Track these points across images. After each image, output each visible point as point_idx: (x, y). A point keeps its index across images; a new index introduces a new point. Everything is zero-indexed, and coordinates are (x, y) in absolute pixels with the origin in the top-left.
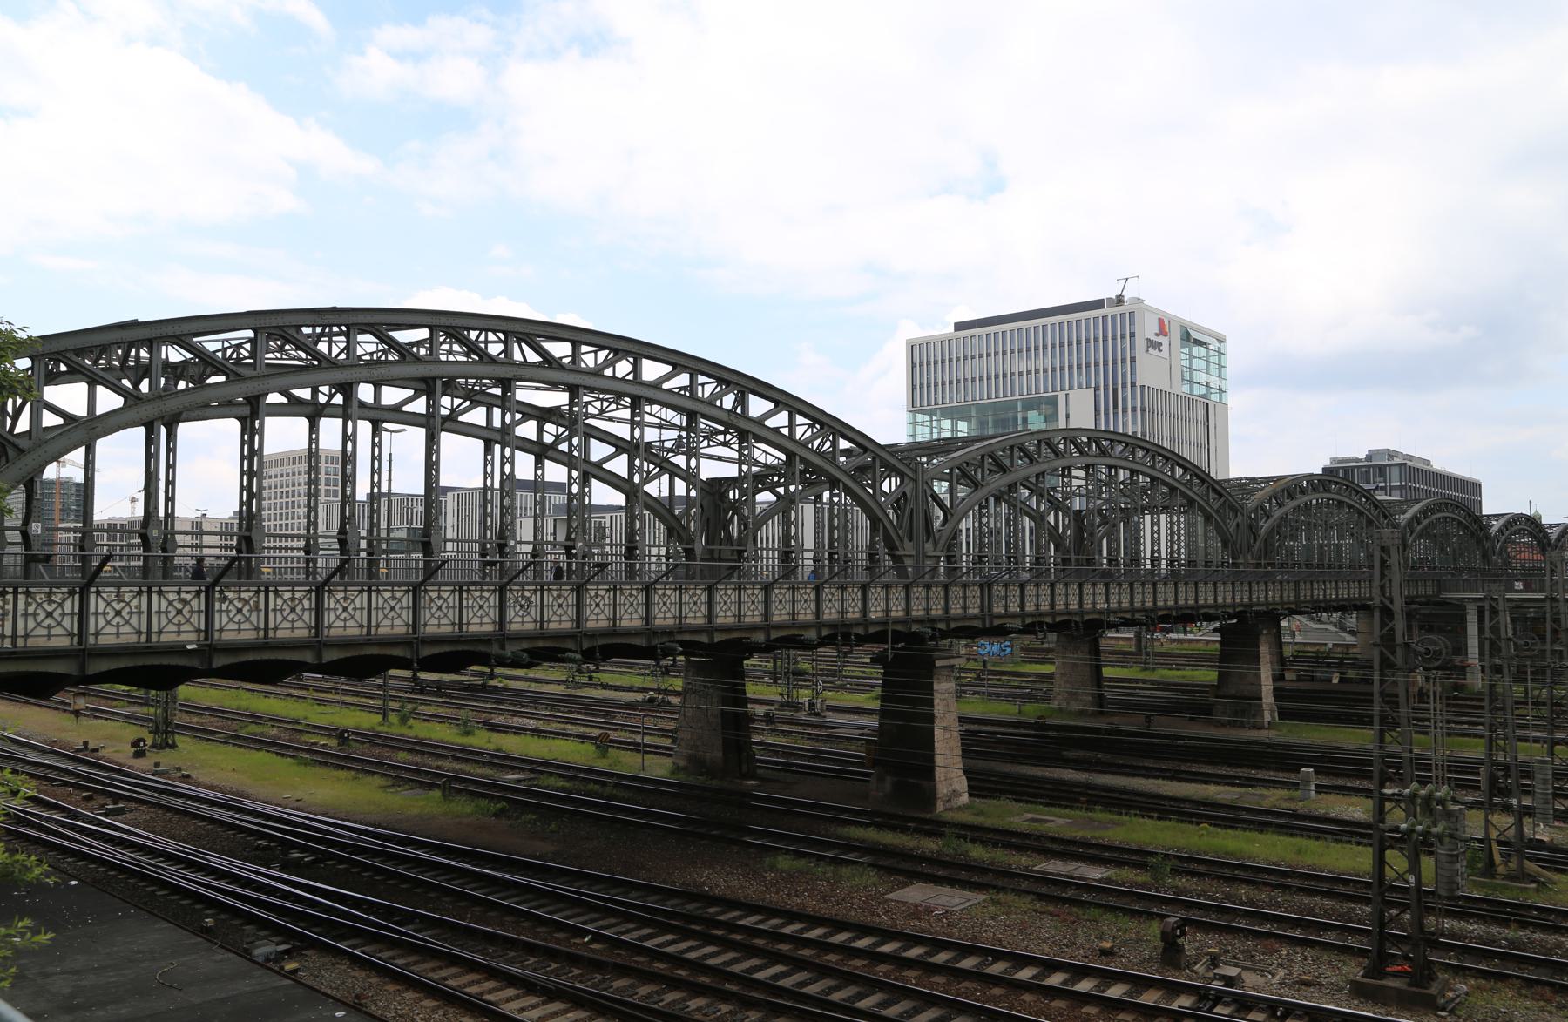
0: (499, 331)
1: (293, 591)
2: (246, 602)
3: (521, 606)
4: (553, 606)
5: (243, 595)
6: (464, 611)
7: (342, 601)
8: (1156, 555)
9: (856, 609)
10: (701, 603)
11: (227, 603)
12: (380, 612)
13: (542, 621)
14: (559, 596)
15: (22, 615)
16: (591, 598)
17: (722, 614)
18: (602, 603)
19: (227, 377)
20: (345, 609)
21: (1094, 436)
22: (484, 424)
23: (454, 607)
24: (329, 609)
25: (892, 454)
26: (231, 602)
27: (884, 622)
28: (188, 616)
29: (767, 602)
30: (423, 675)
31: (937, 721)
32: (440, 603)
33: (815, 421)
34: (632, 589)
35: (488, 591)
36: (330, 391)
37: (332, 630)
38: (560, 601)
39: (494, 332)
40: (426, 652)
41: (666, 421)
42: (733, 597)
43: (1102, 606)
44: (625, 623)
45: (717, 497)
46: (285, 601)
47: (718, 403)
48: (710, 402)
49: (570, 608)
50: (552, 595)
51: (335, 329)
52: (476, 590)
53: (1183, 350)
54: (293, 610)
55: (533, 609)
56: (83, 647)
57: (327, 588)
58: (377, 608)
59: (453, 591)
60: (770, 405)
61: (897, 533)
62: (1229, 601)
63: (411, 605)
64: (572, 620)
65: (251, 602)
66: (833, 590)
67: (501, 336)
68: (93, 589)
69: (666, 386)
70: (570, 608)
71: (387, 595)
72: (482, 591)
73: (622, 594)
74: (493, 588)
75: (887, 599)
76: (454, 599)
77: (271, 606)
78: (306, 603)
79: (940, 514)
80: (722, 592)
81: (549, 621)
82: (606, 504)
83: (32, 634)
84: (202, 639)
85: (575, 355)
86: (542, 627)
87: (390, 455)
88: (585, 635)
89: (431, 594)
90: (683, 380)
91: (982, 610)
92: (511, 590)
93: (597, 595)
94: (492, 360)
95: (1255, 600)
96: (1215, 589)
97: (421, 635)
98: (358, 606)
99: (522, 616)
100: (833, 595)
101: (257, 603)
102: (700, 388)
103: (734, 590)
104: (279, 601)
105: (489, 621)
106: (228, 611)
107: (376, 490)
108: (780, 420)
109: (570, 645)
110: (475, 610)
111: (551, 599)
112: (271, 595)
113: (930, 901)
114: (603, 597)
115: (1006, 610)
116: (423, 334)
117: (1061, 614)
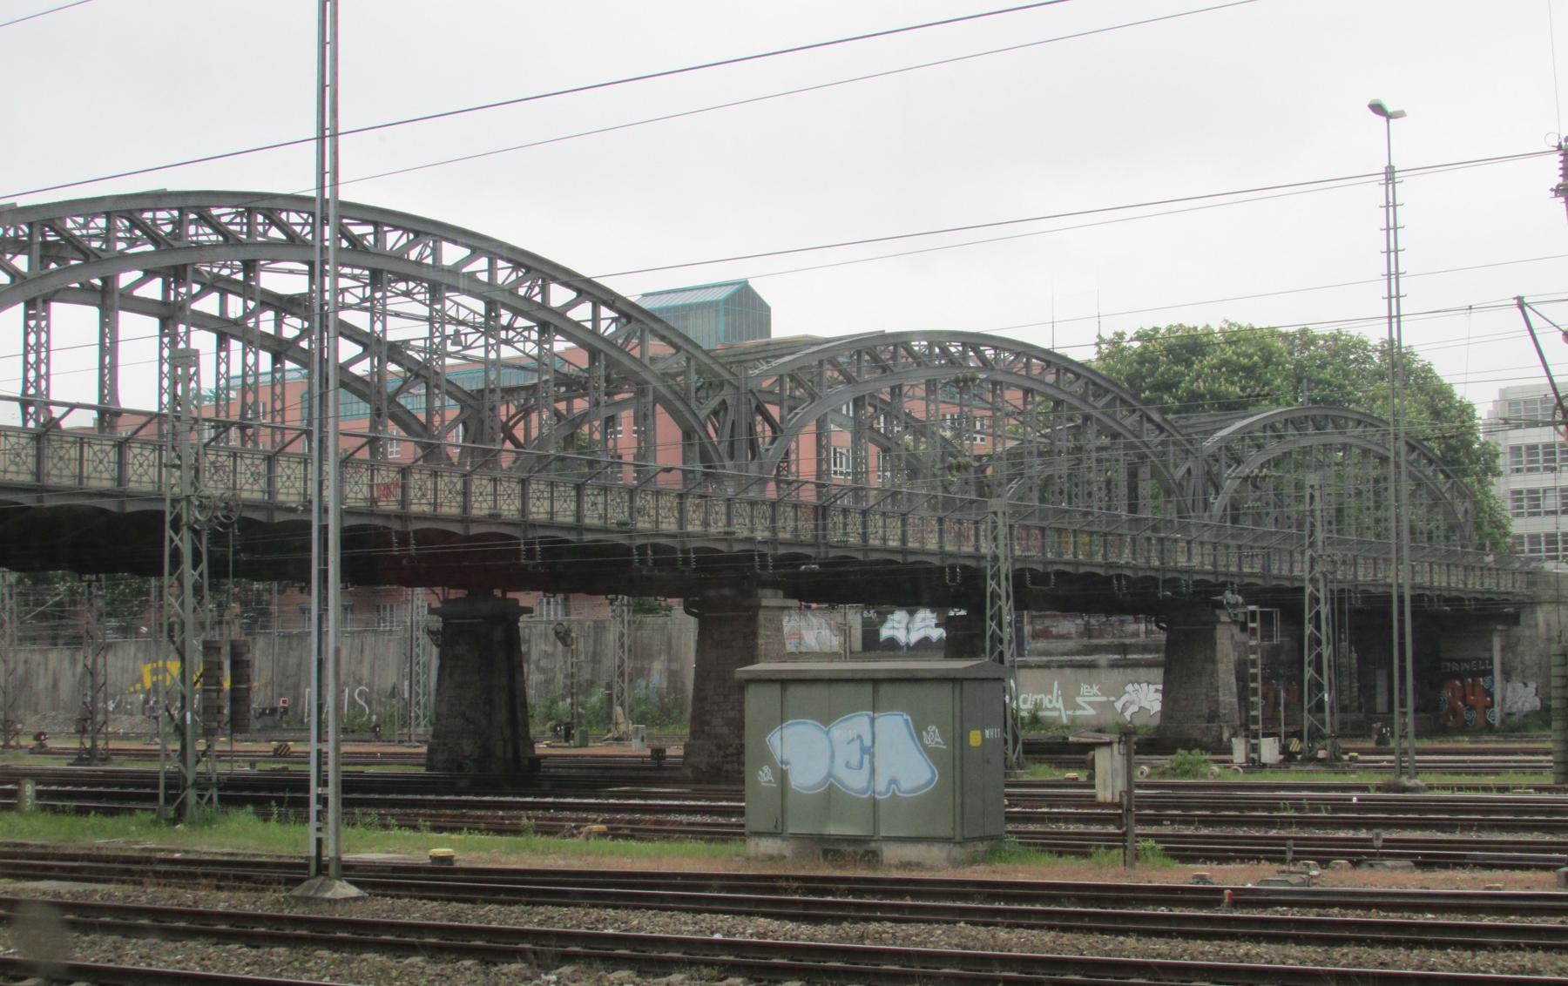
22: (216, 313)
33: (623, 314)
39: (298, 212)
48: (511, 292)
60: (572, 295)
71: (97, 448)
75: (495, 495)
79: (769, 432)
90: (482, 263)
103: (229, 456)
108: (582, 313)
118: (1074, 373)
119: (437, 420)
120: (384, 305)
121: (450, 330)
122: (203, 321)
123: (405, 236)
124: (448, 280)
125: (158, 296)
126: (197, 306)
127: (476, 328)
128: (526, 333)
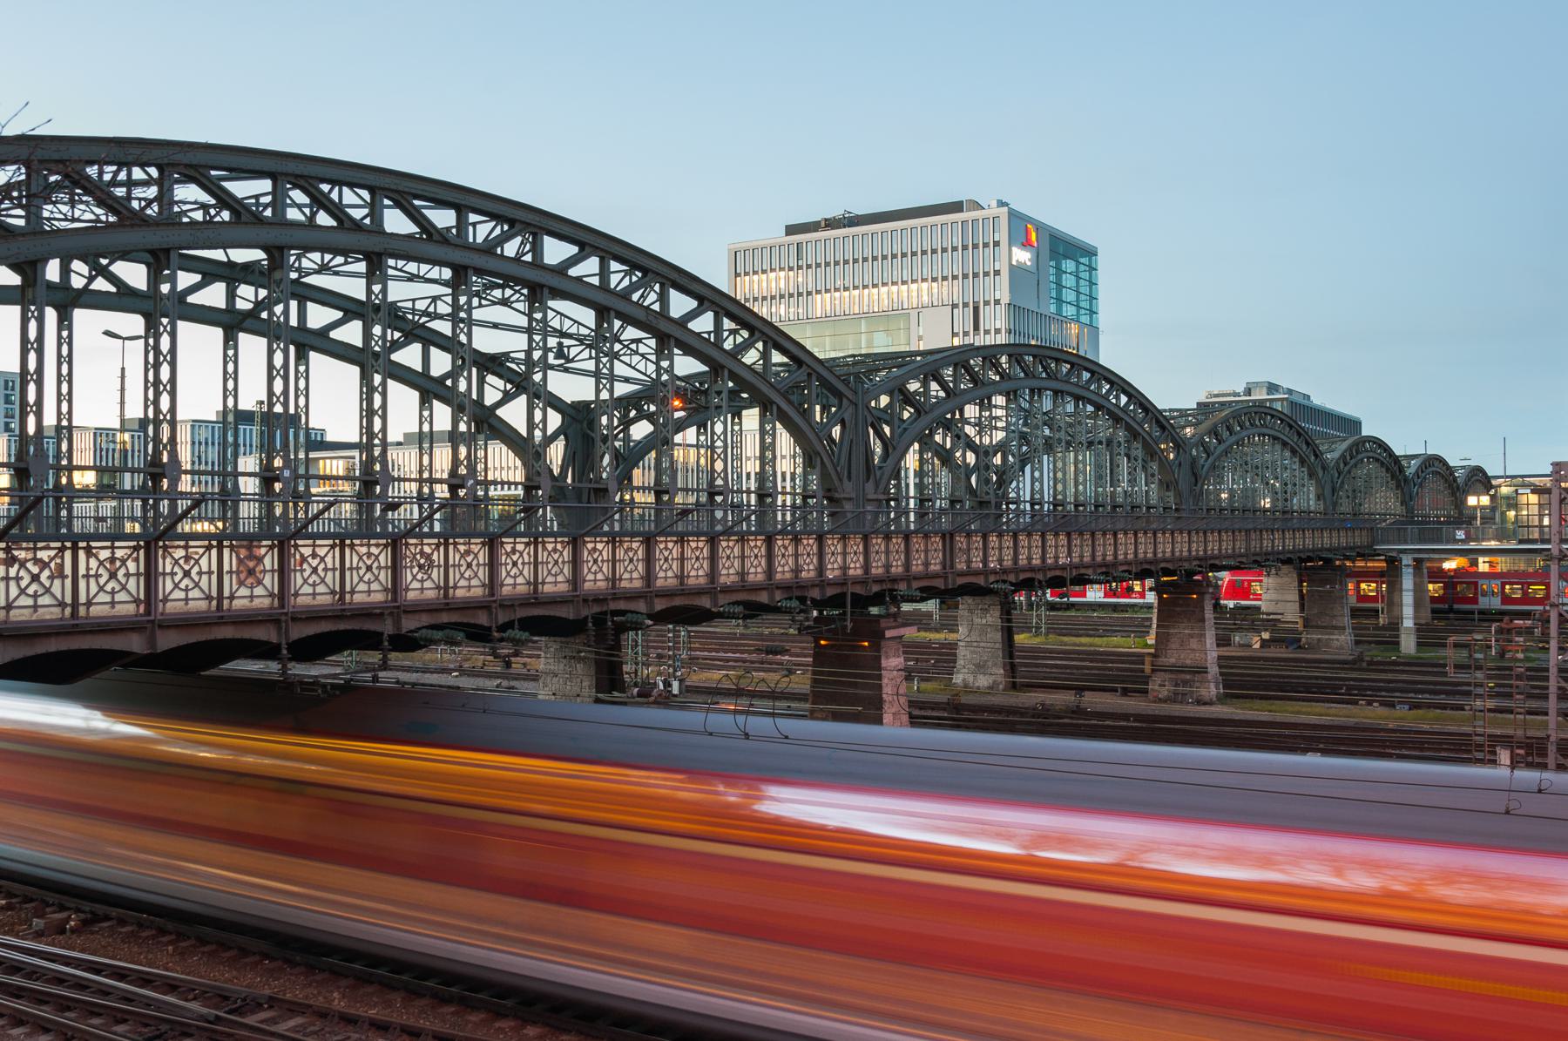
1: (113, 548)
2: (44, 565)
3: (421, 567)
5: (40, 554)
6: (348, 574)
7: (181, 562)
8: (1060, 497)
9: (759, 570)
10: (478, 565)
11: (16, 566)
12: (92, 581)
13: (446, 587)
14: (468, 552)
15: (213, 572)
16: (508, 554)
17: (416, 585)
18: (520, 561)
19: (120, 219)
20: (187, 574)
21: (1015, 352)
24: (164, 574)
25: (829, 369)
26: (23, 564)
27: (843, 582)
28: (123, 581)
29: (649, 560)
31: (886, 706)
32: (314, 563)
34: (556, 542)
35: (377, 545)
36: (90, 272)
37: (169, 605)
38: (469, 559)
40: (299, 632)
41: (645, 374)
43: (1064, 560)
44: (548, 588)
45: (585, 425)
46: (101, 563)
48: (625, 295)
49: (481, 568)
50: (458, 550)
51: (138, 174)
52: (361, 545)
53: (1051, 263)
54: (113, 575)
55: (435, 570)
56: (152, 618)
57: (161, 544)
61: (836, 470)
62: (1008, 563)
64: (484, 585)
65: (52, 565)
66: (787, 542)
69: (573, 272)
70: (481, 568)
72: (369, 545)
73: (544, 548)
74: (384, 541)
76: (334, 557)
77: (82, 571)
78: (132, 566)
80: (662, 546)
81: (455, 587)
82: (111, 136)
83: (16, 604)
84: (442, 596)
87: (123, 369)
88: (502, 606)
89: (303, 550)
92: (407, 544)
93: (514, 551)
94: (357, 226)
95: (1160, 555)
96: (1155, 540)
97: (159, 617)
98: (205, 569)
99: (422, 581)
100: (786, 548)
101: (61, 567)
104: (93, 563)
105: (379, 588)
106: (18, 579)
108: (703, 324)
109: (641, 606)
110: (177, 579)
111: (457, 556)
112: (82, 555)
114: (521, 554)
115: (968, 567)
116: (265, 185)
117: (1024, 570)
118: (1280, 419)
119: (538, 433)
121: (552, 342)
123: (499, 227)
124: (554, 281)
125: (221, 303)
126: (398, 357)
127: (581, 340)
128: (633, 346)
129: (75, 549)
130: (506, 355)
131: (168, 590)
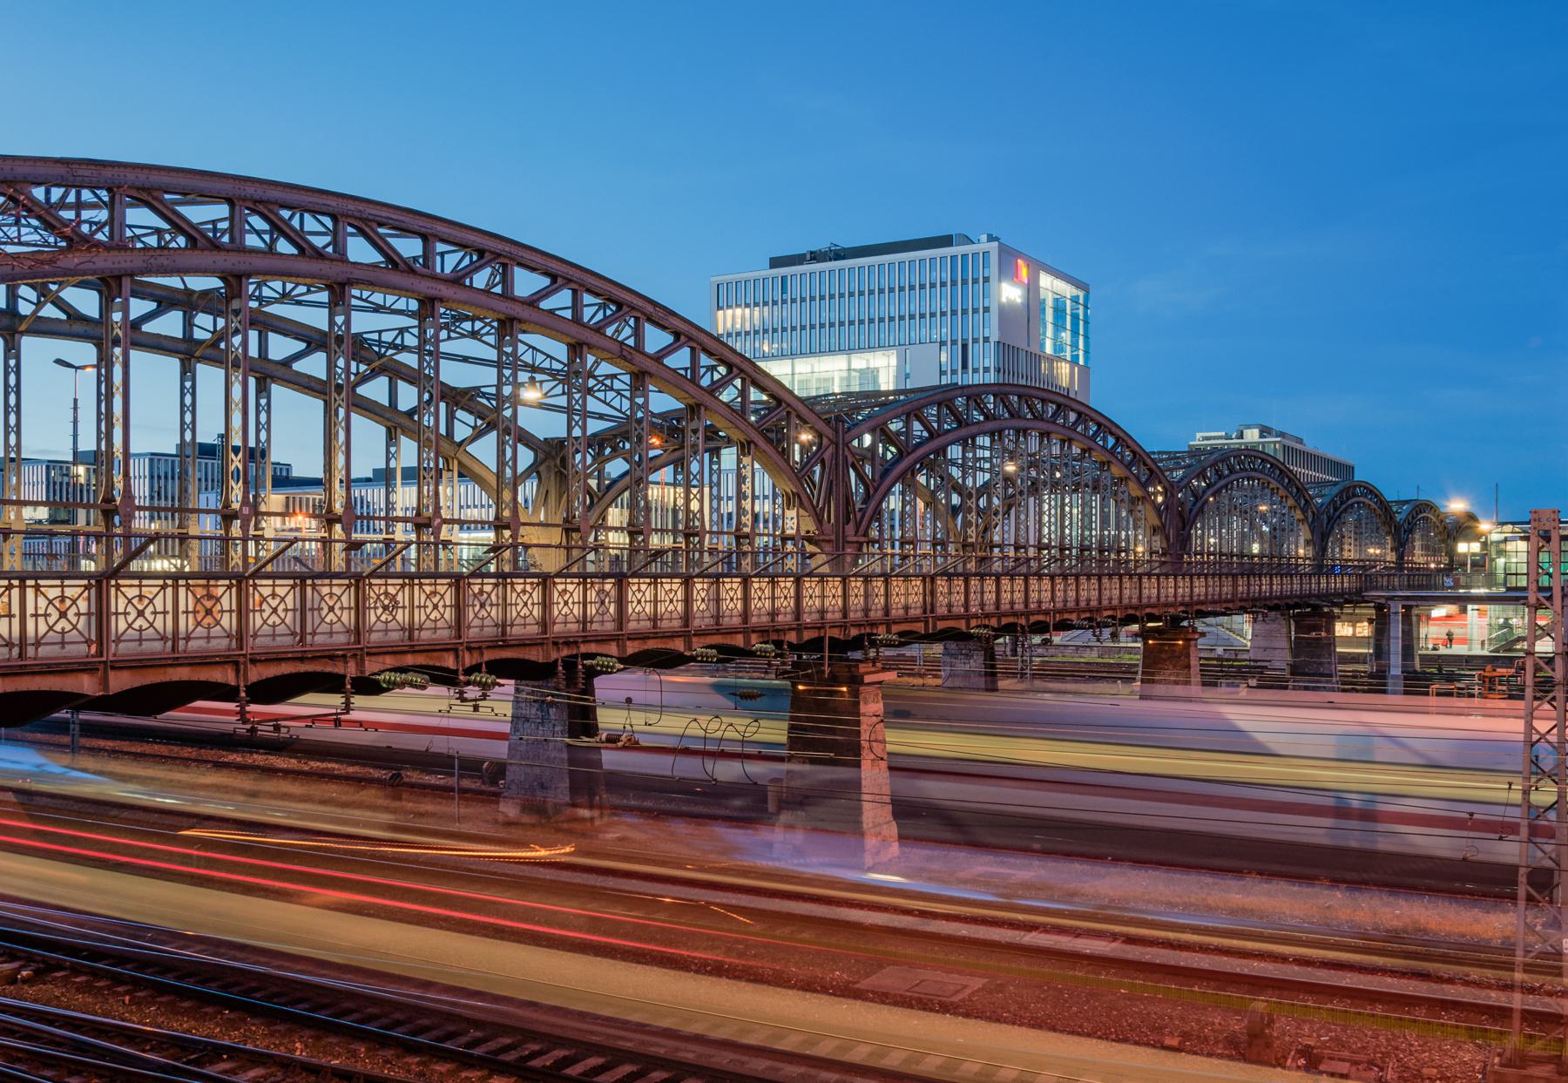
0: (323, 214)
3: (385, 608)
4: (425, 607)
15: (14, 616)
16: (475, 595)
23: (165, 613)
24: (117, 614)
30: (253, 708)
34: (525, 583)
37: (258, 640)
38: (435, 600)
40: (256, 674)
41: (620, 411)
42: (647, 594)
47: (467, 282)
51: (87, 195)
55: (400, 611)
58: (36, 615)
59: (293, 587)
63: (234, 607)
67: (328, 221)
68: (113, 582)
73: (513, 589)
77: (30, 610)
85: (428, 254)
86: (174, 648)
87: (76, 401)
91: (925, 612)
94: (319, 254)
102: (438, 259)
107: (188, 436)
108: (680, 360)
111: (423, 597)
113: (916, 989)
117: (1005, 615)
120: (500, 375)
122: (369, 408)
128: (608, 382)
129: (23, 588)
130: (478, 388)
131: (121, 630)
